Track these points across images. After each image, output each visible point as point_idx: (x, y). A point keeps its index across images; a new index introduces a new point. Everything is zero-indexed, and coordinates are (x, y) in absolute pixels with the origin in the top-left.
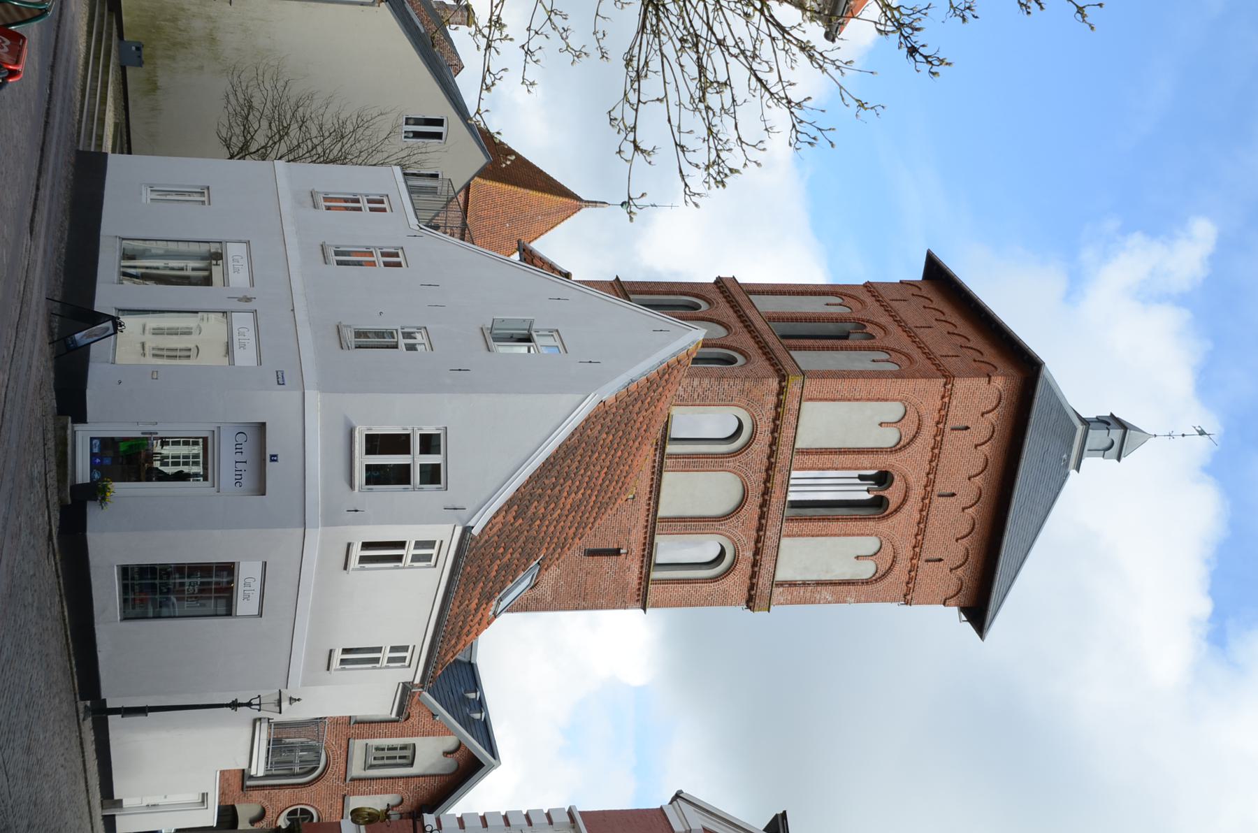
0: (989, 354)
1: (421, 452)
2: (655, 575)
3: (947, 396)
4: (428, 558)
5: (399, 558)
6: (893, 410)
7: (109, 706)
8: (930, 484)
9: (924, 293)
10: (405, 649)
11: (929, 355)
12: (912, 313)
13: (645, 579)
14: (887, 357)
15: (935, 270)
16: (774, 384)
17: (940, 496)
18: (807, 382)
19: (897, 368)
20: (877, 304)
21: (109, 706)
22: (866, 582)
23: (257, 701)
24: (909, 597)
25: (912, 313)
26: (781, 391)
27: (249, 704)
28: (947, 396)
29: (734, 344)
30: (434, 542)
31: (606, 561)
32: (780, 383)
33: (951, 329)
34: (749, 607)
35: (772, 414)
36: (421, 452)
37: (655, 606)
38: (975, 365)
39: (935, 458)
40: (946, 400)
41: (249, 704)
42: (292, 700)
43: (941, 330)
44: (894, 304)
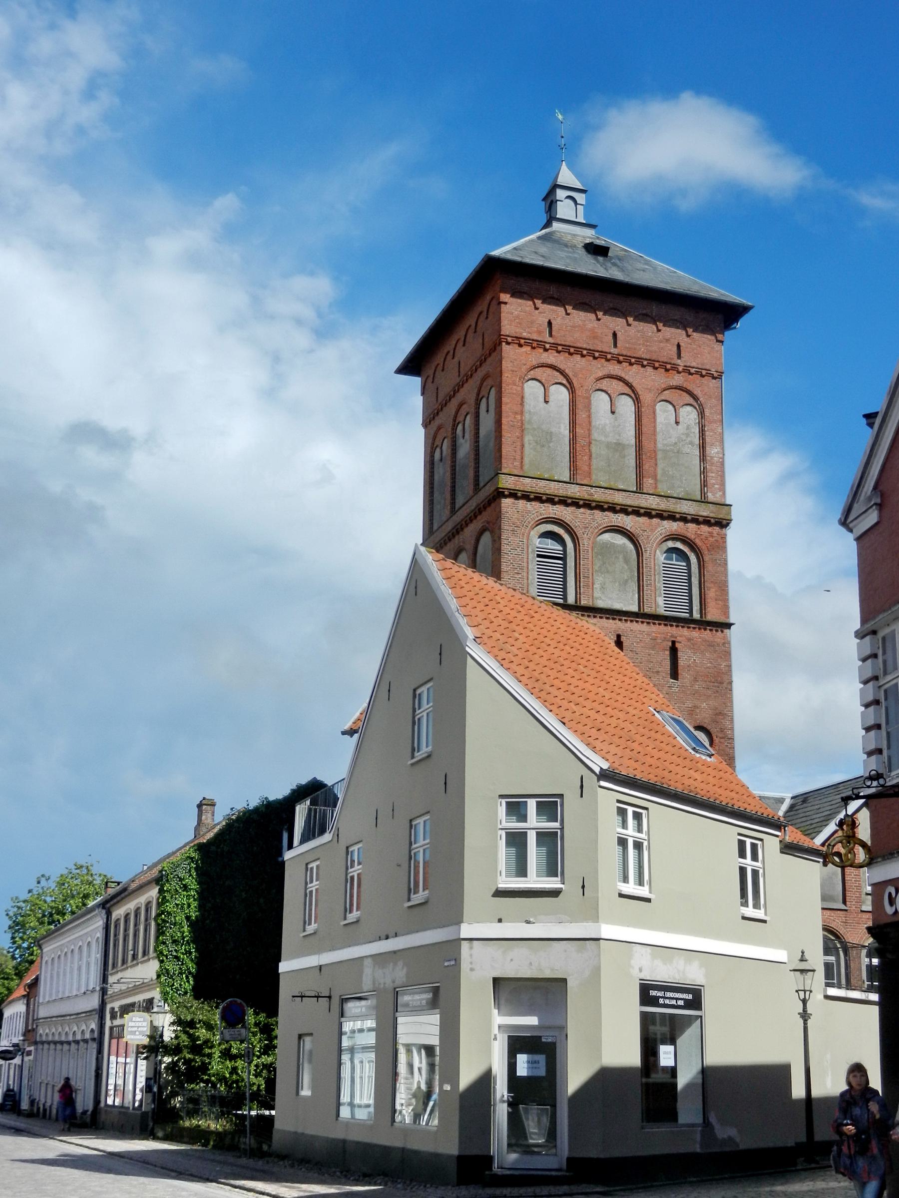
0: (482, 306)
1: (526, 821)
2: (696, 615)
3: (519, 341)
4: (754, 847)
5: (755, 873)
6: (533, 390)
7: (804, 1139)
8: (604, 356)
9: (431, 372)
10: (742, 844)
11: (482, 361)
12: (447, 380)
13: (704, 624)
14: (484, 400)
15: (544, 199)
16: (506, 502)
17: (615, 346)
18: (504, 471)
19: (493, 389)
20: (441, 414)
21: (804, 1139)
22: (702, 414)
23: (802, 994)
24: (716, 374)
25: (447, 380)
26: (514, 495)
27: (804, 1002)
28: (519, 341)
29: (473, 542)
30: (740, 841)
31: (684, 659)
32: (506, 497)
33: (461, 343)
34: (728, 524)
35: (536, 504)
36: (526, 821)
37: (726, 613)
38: (490, 317)
39: (578, 351)
40: (522, 341)
41: (804, 1002)
42: (803, 960)
43: (462, 351)
44: (440, 400)
